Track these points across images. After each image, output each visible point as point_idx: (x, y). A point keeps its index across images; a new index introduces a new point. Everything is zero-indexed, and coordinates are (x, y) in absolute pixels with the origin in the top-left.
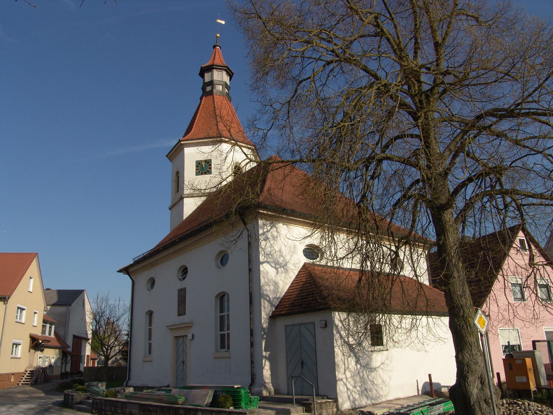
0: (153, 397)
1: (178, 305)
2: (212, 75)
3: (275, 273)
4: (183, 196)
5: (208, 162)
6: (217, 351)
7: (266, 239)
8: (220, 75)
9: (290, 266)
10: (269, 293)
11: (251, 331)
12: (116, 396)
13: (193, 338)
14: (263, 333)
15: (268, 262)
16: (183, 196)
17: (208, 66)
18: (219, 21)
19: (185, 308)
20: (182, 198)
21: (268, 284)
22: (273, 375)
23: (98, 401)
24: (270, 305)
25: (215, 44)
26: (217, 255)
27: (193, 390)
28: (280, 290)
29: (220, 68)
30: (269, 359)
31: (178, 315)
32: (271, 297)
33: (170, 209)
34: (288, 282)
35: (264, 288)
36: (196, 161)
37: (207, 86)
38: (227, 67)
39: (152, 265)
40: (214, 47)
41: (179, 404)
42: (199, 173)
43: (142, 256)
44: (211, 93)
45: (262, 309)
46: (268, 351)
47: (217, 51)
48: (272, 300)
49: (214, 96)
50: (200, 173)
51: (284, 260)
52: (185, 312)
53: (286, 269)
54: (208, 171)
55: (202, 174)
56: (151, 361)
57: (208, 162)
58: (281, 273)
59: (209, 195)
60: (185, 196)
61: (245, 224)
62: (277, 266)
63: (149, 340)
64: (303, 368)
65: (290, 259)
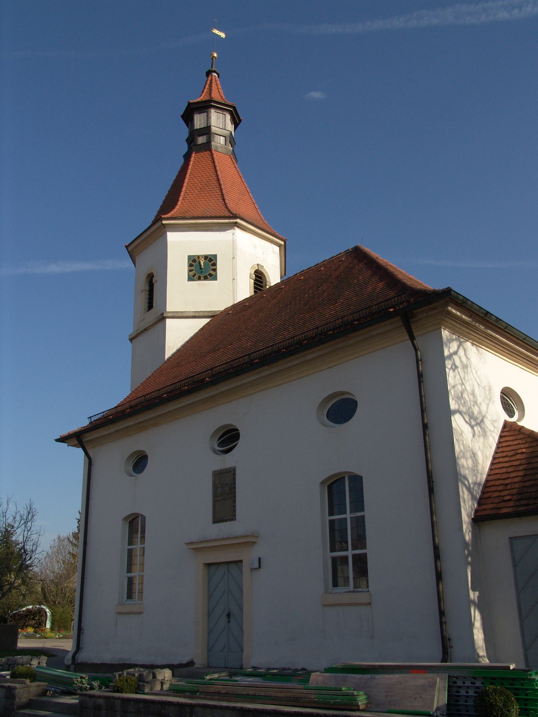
0: (269, 694)
1: (215, 502)
2: (208, 118)
3: (471, 435)
4: (165, 315)
5: (211, 260)
6: (326, 591)
7: (455, 367)
8: (221, 120)
9: (488, 423)
10: (467, 472)
11: (436, 548)
12: (139, 689)
13: (260, 566)
14: (466, 552)
15: (460, 413)
16: (165, 315)
17: (202, 102)
18: (216, 31)
19: (234, 507)
20: (162, 318)
21: (464, 457)
22: (487, 639)
23: (101, 701)
24: (470, 496)
25: (210, 68)
26: (322, 402)
27: (377, 676)
28: (480, 468)
29: (222, 107)
30: (481, 606)
31: (214, 522)
32: (470, 481)
33: (131, 340)
34: (488, 454)
35: (460, 463)
36: (190, 257)
37: (199, 136)
38: (234, 108)
39: (141, 427)
40: (209, 73)
41: (358, 710)
42: (194, 276)
43: (100, 416)
44: (207, 147)
45: (462, 504)
46: (477, 591)
47: (214, 81)
48: (472, 486)
49: (214, 152)
50: (197, 276)
51: (480, 412)
52: (235, 515)
53: (484, 429)
54: (211, 275)
55: (199, 279)
56: (141, 613)
57: (211, 260)
58: (479, 437)
59: (213, 316)
60: (169, 315)
61: (412, 338)
62: (473, 423)
63: (128, 572)
64: (229, 622)
65: (487, 412)
